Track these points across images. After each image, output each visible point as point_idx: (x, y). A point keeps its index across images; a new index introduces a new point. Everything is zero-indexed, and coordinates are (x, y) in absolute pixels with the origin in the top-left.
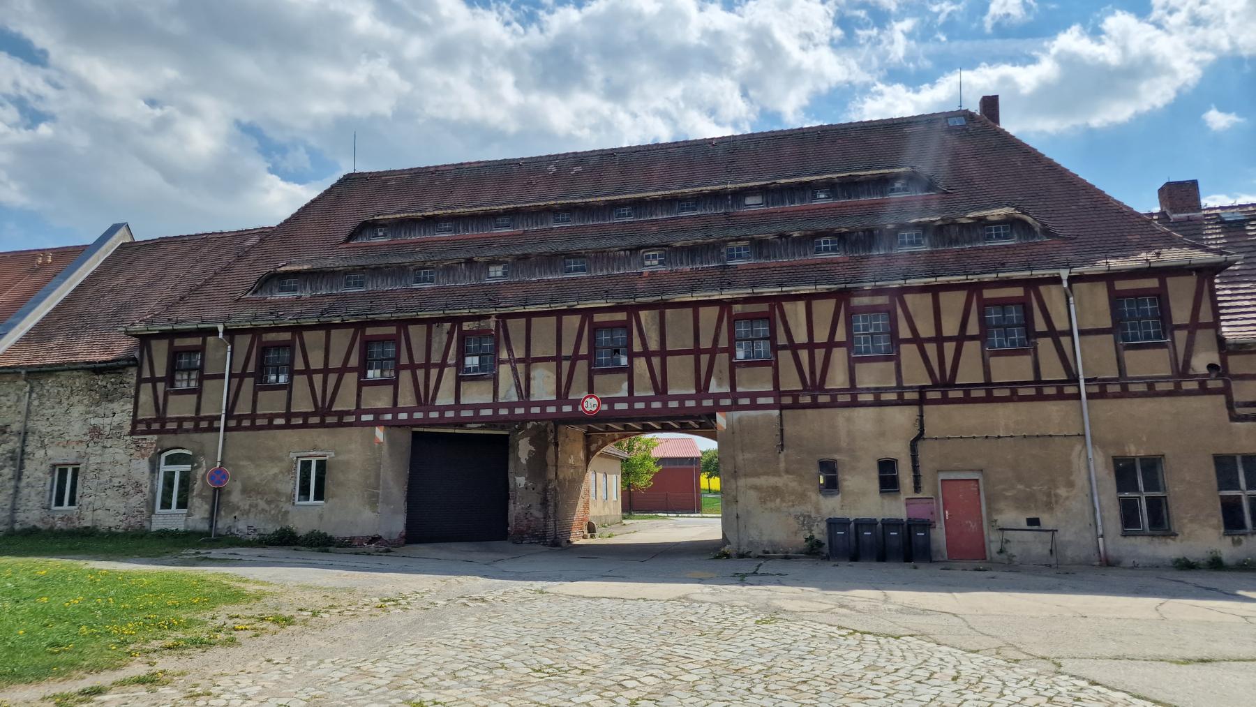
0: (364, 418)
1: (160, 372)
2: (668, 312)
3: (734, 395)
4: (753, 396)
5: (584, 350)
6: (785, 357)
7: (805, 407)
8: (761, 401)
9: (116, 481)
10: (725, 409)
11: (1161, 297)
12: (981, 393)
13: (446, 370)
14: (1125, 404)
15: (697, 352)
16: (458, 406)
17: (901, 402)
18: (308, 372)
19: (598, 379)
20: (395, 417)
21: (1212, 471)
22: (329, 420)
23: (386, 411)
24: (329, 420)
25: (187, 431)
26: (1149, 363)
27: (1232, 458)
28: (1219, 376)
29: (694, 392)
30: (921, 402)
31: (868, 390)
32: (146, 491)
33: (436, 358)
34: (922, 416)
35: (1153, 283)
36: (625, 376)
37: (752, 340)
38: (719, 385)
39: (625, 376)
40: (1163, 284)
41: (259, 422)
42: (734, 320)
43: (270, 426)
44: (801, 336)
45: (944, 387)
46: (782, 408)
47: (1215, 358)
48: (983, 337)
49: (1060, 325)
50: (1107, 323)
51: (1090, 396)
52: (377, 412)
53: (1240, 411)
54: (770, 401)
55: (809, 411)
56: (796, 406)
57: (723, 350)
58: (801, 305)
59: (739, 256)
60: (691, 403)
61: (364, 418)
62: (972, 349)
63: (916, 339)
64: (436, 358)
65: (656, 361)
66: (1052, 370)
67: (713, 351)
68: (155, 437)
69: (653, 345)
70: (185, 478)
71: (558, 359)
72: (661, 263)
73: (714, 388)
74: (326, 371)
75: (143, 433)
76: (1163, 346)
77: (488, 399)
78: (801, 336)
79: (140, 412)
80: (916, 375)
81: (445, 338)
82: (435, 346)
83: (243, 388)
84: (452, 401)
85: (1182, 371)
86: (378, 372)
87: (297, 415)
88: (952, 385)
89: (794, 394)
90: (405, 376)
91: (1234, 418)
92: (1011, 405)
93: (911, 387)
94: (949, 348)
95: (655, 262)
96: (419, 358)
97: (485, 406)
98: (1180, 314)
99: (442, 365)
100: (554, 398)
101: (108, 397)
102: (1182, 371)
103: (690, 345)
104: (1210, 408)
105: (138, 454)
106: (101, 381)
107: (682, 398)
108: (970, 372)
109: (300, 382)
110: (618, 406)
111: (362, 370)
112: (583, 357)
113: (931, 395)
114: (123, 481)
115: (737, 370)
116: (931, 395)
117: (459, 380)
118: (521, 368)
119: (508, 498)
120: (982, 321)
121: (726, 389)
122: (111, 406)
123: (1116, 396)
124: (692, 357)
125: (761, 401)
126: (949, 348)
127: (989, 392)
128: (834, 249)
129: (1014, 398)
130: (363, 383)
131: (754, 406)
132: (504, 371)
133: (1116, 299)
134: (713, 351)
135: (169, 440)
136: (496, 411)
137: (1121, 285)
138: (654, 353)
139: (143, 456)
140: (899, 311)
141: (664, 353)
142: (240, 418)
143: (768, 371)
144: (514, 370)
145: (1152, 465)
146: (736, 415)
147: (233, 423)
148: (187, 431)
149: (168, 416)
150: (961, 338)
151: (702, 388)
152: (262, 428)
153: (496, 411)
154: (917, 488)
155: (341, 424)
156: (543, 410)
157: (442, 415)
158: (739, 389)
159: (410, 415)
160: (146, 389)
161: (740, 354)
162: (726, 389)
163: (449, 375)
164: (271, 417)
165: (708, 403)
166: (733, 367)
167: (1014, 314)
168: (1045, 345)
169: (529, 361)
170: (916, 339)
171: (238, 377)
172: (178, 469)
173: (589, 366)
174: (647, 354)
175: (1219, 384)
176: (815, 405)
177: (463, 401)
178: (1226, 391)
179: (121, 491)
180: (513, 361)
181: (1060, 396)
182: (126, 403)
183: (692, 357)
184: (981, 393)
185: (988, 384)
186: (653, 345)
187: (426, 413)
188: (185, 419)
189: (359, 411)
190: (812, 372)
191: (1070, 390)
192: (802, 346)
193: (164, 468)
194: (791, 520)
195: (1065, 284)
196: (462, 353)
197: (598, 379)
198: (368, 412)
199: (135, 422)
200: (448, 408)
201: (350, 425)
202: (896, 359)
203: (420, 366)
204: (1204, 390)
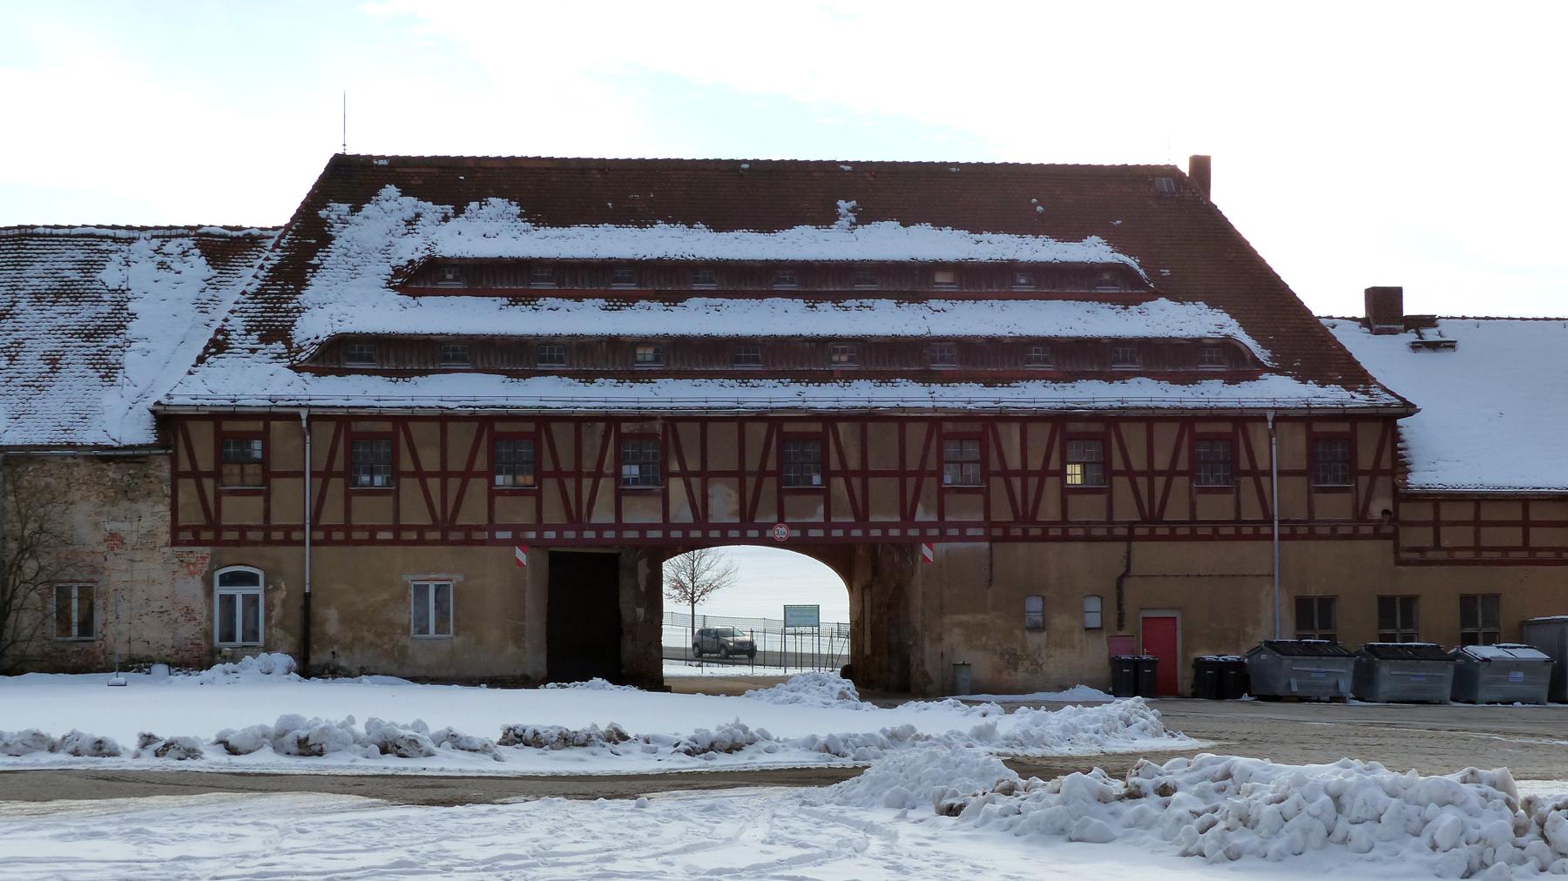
0: (500, 535)
1: (206, 463)
2: (870, 425)
3: (941, 524)
4: (962, 526)
5: (771, 465)
6: (997, 485)
7: (1017, 539)
8: (970, 532)
9: (155, 606)
10: (930, 542)
11: (1350, 441)
12: (1230, 531)
13: (602, 481)
14: (1311, 545)
15: (902, 474)
16: (619, 526)
17: (1112, 538)
18: (420, 475)
19: (789, 500)
20: (540, 535)
21: (1375, 612)
22: (1160, 531)
23: (527, 528)
24: (453, 536)
25: (255, 543)
26: (1334, 507)
27: (1392, 599)
28: (1390, 522)
29: (897, 519)
30: (1130, 538)
31: (363, 528)
32: (202, 618)
33: (589, 465)
34: (1129, 552)
35: (1344, 427)
36: (821, 498)
37: (961, 463)
38: (927, 512)
39: (821, 498)
40: (1354, 431)
41: (356, 535)
42: (944, 438)
43: (372, 541)
44: (1015, 463)
45: (1152, 523)
46: (993, 540)
47: (1389, 505)
48: (1191, 474)
49: (1262, 465)
50: (1302, 465)
51: (1282, 537)
52: (517, 529)
53: (1404, 556)
54: (980, 532)
55: (363, 548)
56: (1006, 538)
57: (932, 474)
58: (1015, 429)
59: (942, 360)
60: (894, 532)
61: (500, 535)
62: (1181, 483)
63: (1130, 473)
64: (589, 465)
65: (856, 482)
66: (1252, 511)
67: (920, 474)
68: (207, 550)
69: (854, 463)
70: (251, 601)
71: (741, 474)
72: (851, 360)
73: (920, 516)
74: (444, 474)
75: (189, 543)
76: (1346, 490)
77: (658, 519)
78: (1015, 463)
79: (181, 515)
80: (1126, 510)
81: (599, 442)
82: (586, 450)
83: (330, 490)
84: (611, 519)
85: (1361, 515)
86: (509, 479)
87: (410, 528)
88: (1159, 521)
89: (1005, 526)
90: (550, 485)
91: (1399, 562)
92: (1211, 544)
93: (1079, 523)
94: (1160, 482)
95: (844, 358)
96: (567, 464)
97: (653, 527)
98: (1365, 460)
99: (597, 475)
100: (737, 520)
101: (126, 493)
102: (1361, 515)
103: (894, 465)
104: (1374, 552)
105: (185, 571)
106: (112, 472)
107: (884, 527)
108: (1177, 510)
109: (409, 487)
110: (813, 533)
111: (490, 476)
112: (771, 474)
113: (1140, 531)
114: (167, 605)
115: (946, 497)
116: (1140, 531)
117: (619, 495)
118: (695, 482)
119: (620, 632)
120: (349, 455)
121: (933, 518)
122: (134, 506)
123: (1305, 538)
124: (871, 480)
125: (970, 532)
126: (1160, 482)
127: (1193, 530)
128: (1046, 361)
129: (1215, 537)
130: (493, 493)
131: (963, 538)
132: (676, 486)
133: (1313, 440)
134: (920, 474)
135: (228, 553)
136: (828, 532)
137: (1318, 428)
138: (855, 473)
139: (192, 574)
140: (1114, 440)
141: (865, 473)
142: (328, 529)
143: (979, 499)
144: (688, 486)
145: (1327, 603)
146: (941, 547)
147: (320, 535)
148: (255, 543)
149: (224, 523)
150: (1171, 473)
151: (907, 517)
152: (359, 543)
153: (828, 532)
154: (1120, 626)
155: (469, 542)
156: (885, 532)
157: (599, 535)
158: (948, 518)
159: (559, 534)
160: (187, 489)
161: (948, 479)
162: (933, 518)
163: (606, 486)
164: (373, 530)
165: (913, 532)
166: (942, 492)
167: (384, 449)
168: (1247, 483)
169: (705, 475)
170: (1130, 473)
171: (324, 476)
172: (239, 592)
173: (346, 486)
174: (846, 474)
175: (1389, 529)
176: (1026, 538)
177: (627, 519)
178: (1394, 536)
179: (165, 617)
180: (685, 474)
181: (1257, 537)
182: (156, 503)
183: (871, 480)
184: (1230, 531)
185: (1193, 521)
186: (854, 463)
187: (580, 532)
188: (250, 528)
189: (492, 526)
190: (1025, 503)
191: (1265, 530)
192: (1016, 473)
193: (220, 591)
194: (996, 659)
195: (304, 424)
196: (620, 461)
197: (789, 500)
198: (504, 528)
199: (175, 529)
200: (608, 527)
201: (482, 543)
202: (1109, 492)
203: (568, 475)
204: (1377, 535)
